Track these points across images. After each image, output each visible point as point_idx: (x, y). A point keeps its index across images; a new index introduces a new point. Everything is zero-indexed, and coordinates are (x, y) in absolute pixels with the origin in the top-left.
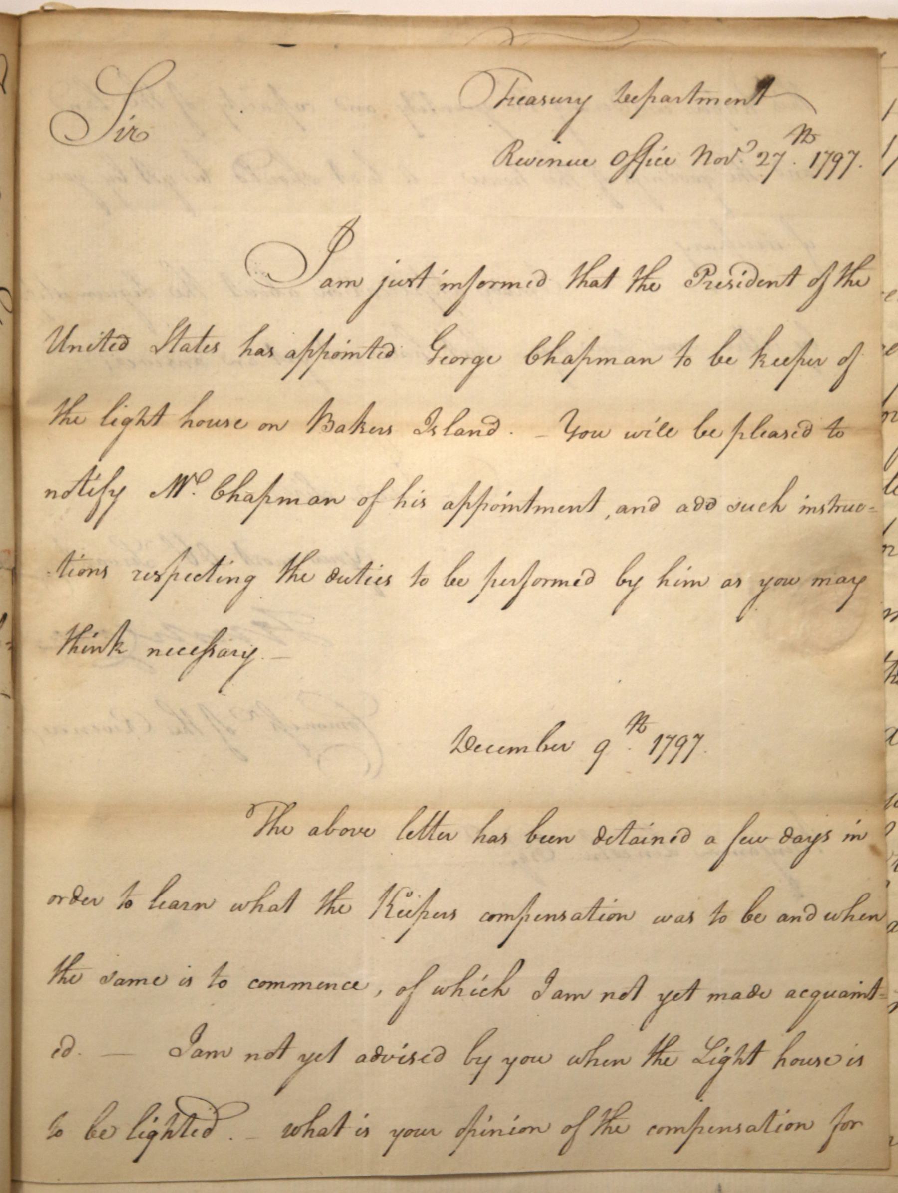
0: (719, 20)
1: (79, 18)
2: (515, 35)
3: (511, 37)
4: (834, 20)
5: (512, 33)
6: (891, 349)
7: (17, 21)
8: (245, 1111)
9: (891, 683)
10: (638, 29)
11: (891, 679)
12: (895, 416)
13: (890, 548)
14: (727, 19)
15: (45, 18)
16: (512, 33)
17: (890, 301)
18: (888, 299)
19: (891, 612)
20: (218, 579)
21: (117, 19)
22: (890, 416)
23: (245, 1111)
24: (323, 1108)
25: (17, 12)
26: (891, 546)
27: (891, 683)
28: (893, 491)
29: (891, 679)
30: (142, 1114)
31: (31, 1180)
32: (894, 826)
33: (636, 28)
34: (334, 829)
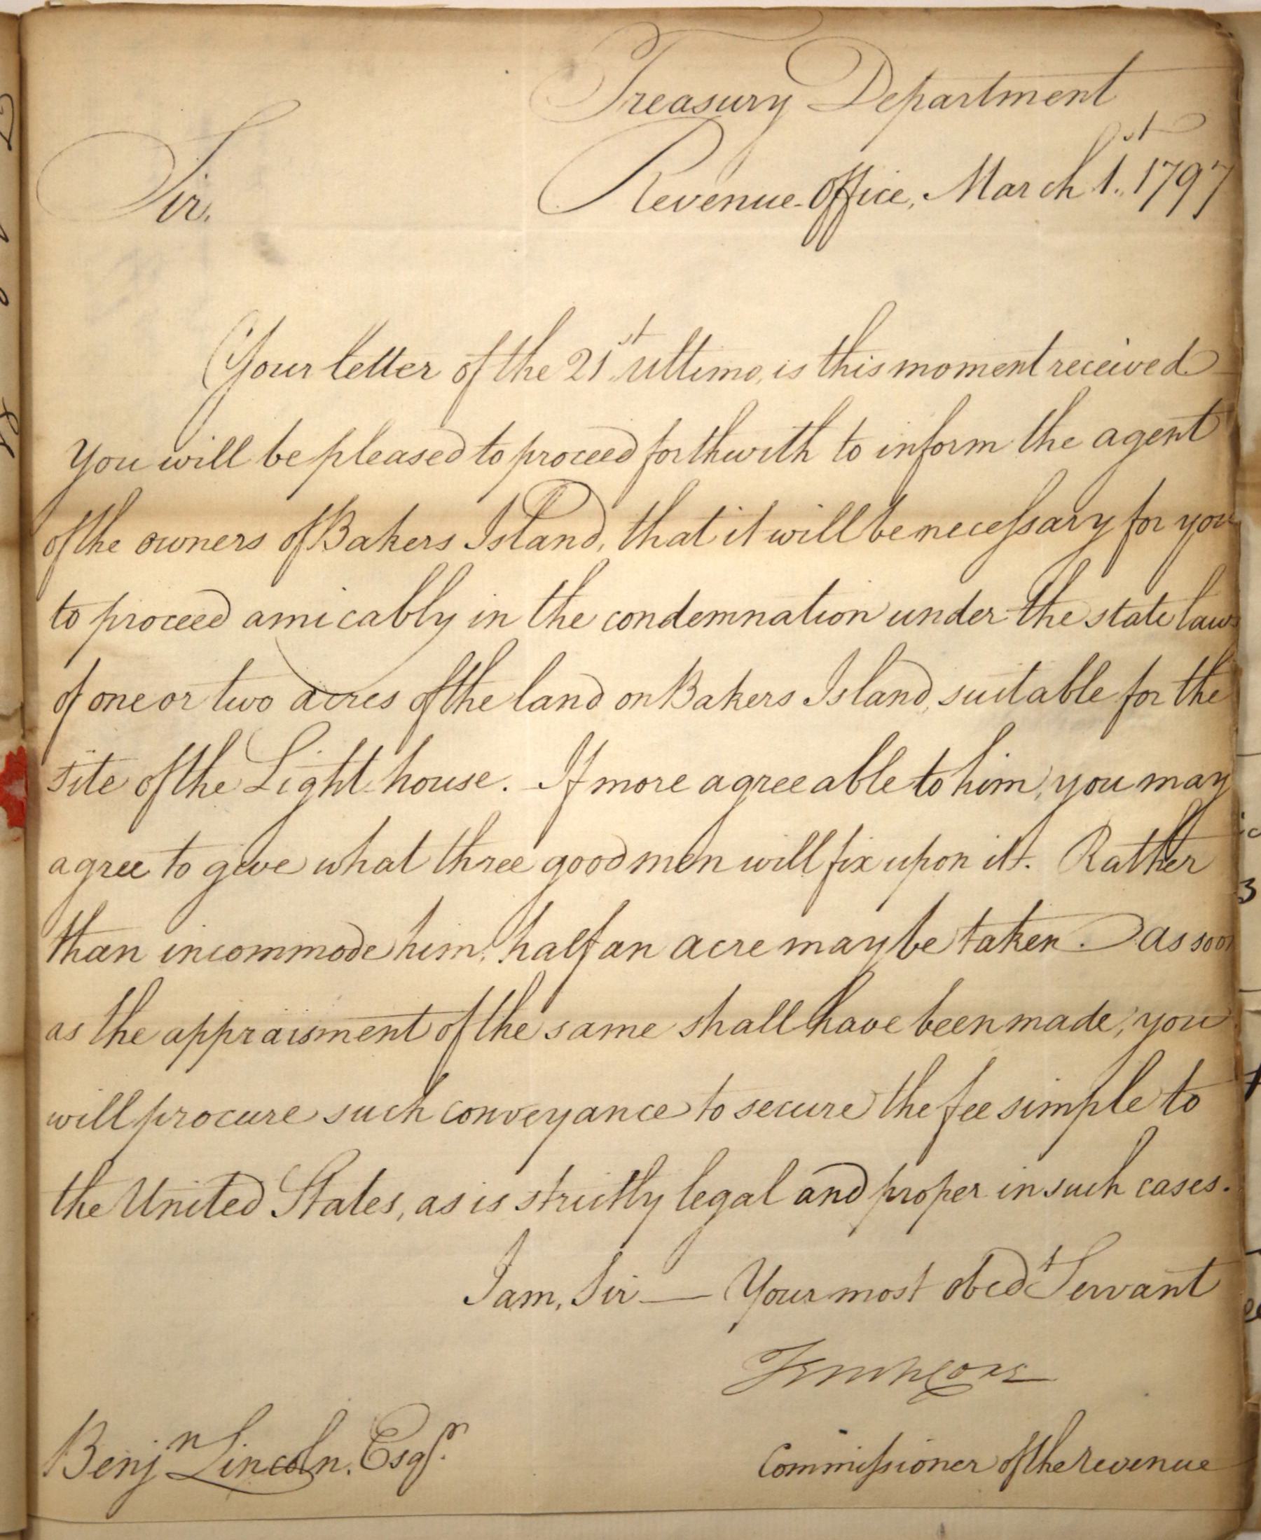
0: (927, 10)
1: (96, 15)
2: (661, 32)
3: (656, 35)
4: (1076, 9)
5: (658, 31)
6: (1153, 436)
7: (16, 23)
8: (687, 1112)
9: (1158, 869)
10: (822, 21)
11: (1157, 865)
12: (1158, 523)
13: (1155, 695)
14: (937, 10)
15: (51, 16)
16: (658, 31)
17: (1151, 374)
18: (1149, 371)
19: (1157, 778)
20: (313, 784)
21: (143, 16)
22: (1153, 524)
23: (687, 1112)
24: (1145, 528)
25: (18, 12)
26: (1155, 692)
27: (1158, 869)
28: (1158, 621)
29: (1157, 865)
30: (1181, 817)
31: (49, 1517)
32: (1163, 1056)
33: (818, 22)
34: (975, 1288)
